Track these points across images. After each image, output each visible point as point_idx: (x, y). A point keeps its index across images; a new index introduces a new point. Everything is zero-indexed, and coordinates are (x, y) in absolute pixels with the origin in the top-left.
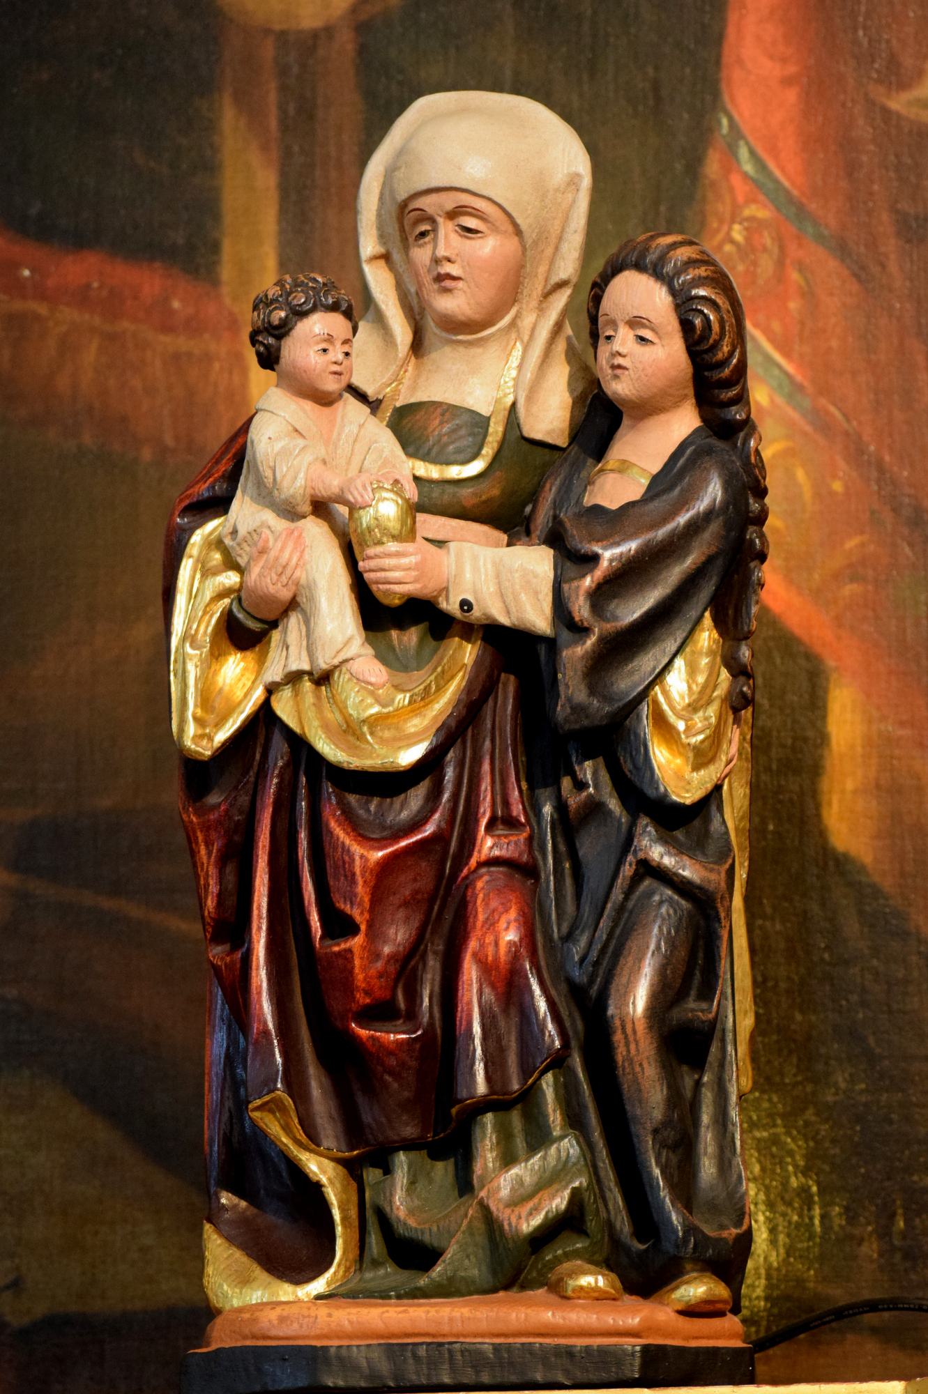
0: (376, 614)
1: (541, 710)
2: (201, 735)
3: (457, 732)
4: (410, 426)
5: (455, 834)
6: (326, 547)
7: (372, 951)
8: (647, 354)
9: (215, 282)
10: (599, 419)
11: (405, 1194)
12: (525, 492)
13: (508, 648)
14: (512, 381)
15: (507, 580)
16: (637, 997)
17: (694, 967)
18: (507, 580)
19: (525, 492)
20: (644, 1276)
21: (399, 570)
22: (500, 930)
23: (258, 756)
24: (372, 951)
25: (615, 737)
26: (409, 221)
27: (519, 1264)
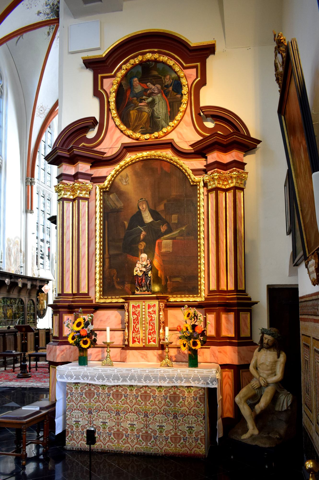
0: (140, 271)
1: (145, 274)
2: (135, 274)
3: (143, 274)
4: (142, 265)
5: (85, 304)
6: (138, 269)
7: (140, 282)
8: (149, 262)
9: (189, 367)
10: (147, 264)
11: (141, 289)
12: (145, 267)
13: (144, 272)
14: (145, 263)
15: (144, 269)
16: (148, 283)
17: (150, 282)
18: (144, 269)
19: (145, 267)
20: (148, 291)
21: (141, 270)
22: (144, 281)
23: (218, 296)
24: (140, 282)
25: (147, 275)
26: (141, 258)
27: (144, 291)
